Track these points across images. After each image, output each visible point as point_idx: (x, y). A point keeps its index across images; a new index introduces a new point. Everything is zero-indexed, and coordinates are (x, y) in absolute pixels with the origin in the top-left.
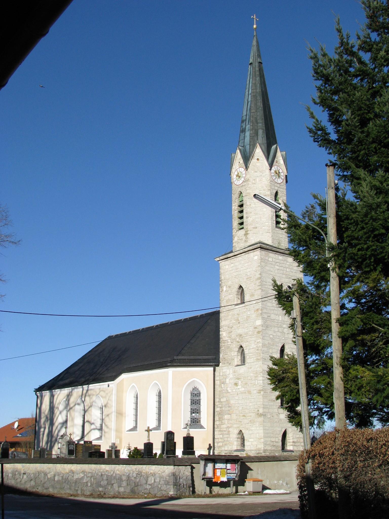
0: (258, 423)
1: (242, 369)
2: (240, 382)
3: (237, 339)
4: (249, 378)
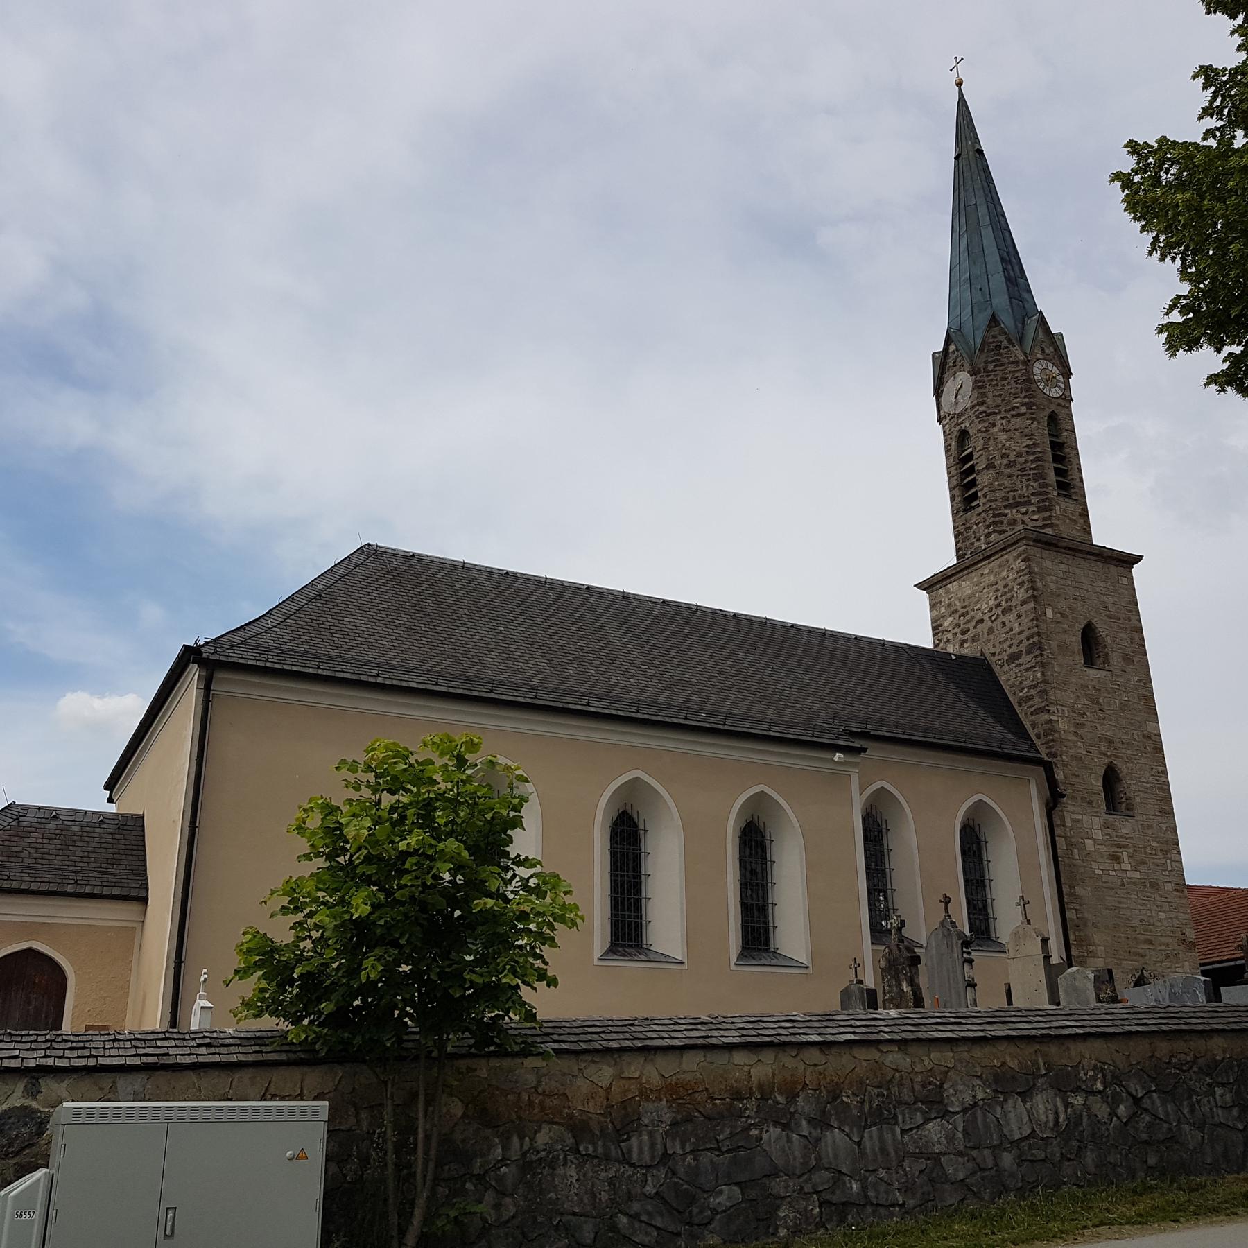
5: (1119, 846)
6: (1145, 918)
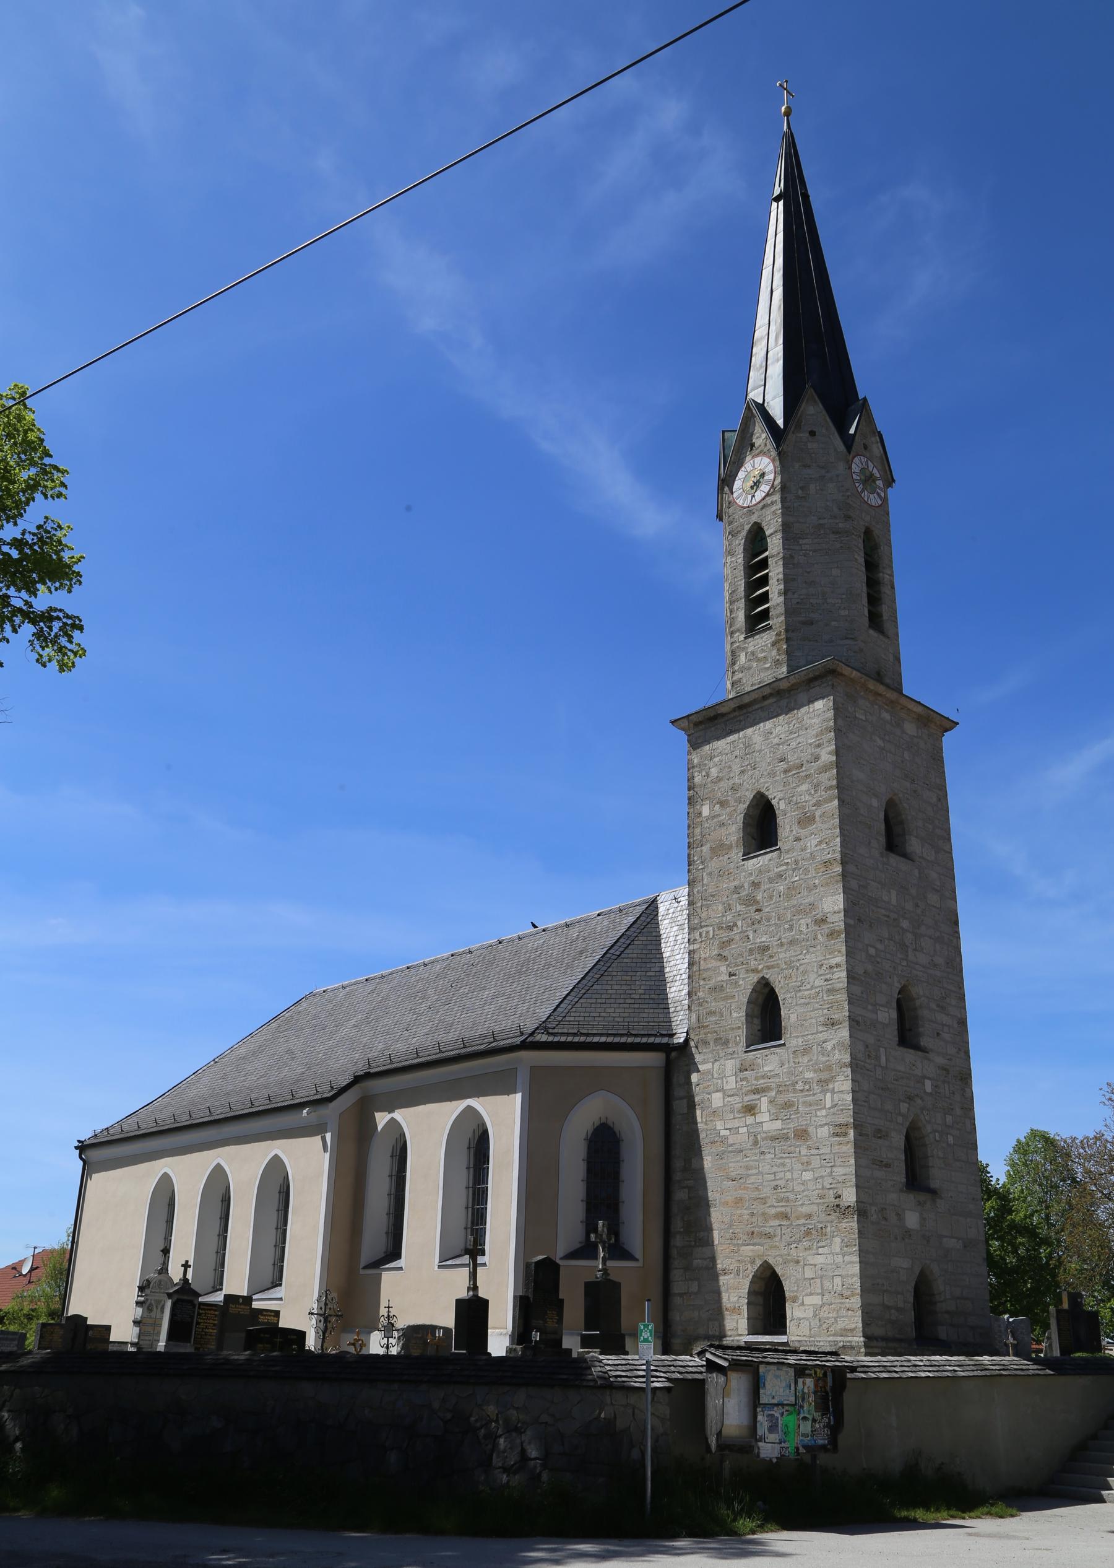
0: (837, 1240)
1: (771, 1061)
2: (764, 1100)
3: (753, 963)
4: (799, 1086)
5: (756, 1091)
6: (781, 1183)
